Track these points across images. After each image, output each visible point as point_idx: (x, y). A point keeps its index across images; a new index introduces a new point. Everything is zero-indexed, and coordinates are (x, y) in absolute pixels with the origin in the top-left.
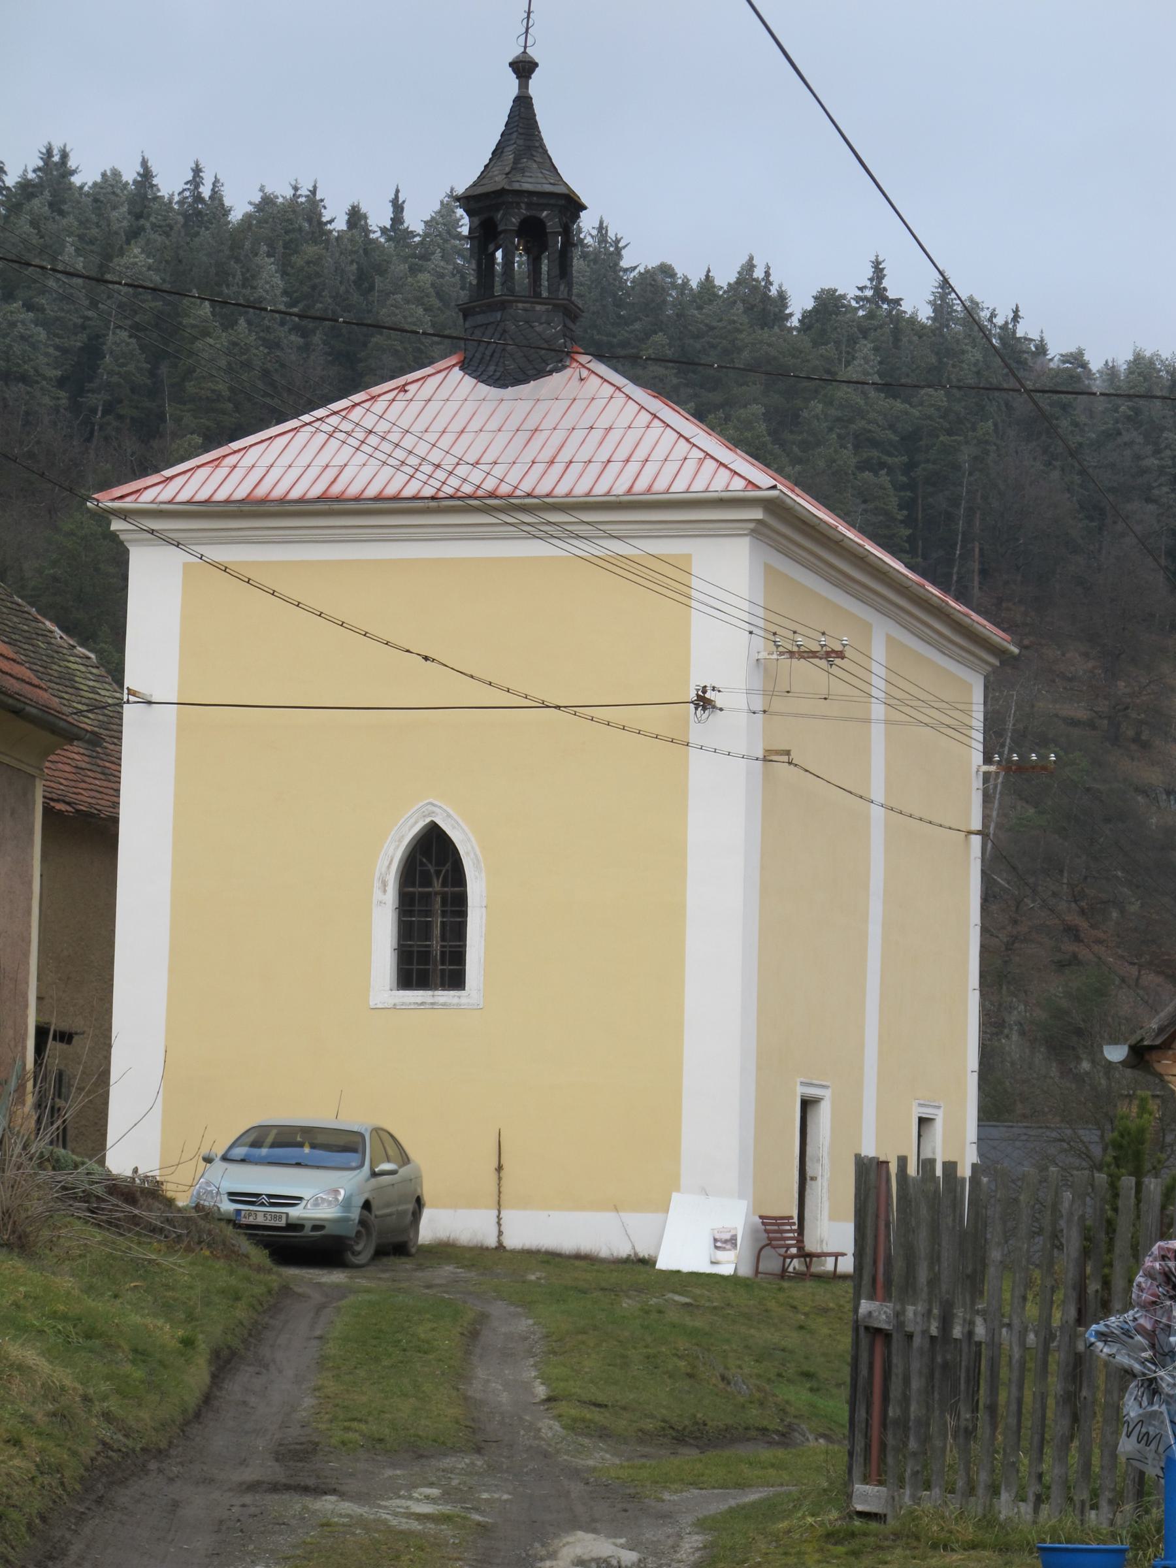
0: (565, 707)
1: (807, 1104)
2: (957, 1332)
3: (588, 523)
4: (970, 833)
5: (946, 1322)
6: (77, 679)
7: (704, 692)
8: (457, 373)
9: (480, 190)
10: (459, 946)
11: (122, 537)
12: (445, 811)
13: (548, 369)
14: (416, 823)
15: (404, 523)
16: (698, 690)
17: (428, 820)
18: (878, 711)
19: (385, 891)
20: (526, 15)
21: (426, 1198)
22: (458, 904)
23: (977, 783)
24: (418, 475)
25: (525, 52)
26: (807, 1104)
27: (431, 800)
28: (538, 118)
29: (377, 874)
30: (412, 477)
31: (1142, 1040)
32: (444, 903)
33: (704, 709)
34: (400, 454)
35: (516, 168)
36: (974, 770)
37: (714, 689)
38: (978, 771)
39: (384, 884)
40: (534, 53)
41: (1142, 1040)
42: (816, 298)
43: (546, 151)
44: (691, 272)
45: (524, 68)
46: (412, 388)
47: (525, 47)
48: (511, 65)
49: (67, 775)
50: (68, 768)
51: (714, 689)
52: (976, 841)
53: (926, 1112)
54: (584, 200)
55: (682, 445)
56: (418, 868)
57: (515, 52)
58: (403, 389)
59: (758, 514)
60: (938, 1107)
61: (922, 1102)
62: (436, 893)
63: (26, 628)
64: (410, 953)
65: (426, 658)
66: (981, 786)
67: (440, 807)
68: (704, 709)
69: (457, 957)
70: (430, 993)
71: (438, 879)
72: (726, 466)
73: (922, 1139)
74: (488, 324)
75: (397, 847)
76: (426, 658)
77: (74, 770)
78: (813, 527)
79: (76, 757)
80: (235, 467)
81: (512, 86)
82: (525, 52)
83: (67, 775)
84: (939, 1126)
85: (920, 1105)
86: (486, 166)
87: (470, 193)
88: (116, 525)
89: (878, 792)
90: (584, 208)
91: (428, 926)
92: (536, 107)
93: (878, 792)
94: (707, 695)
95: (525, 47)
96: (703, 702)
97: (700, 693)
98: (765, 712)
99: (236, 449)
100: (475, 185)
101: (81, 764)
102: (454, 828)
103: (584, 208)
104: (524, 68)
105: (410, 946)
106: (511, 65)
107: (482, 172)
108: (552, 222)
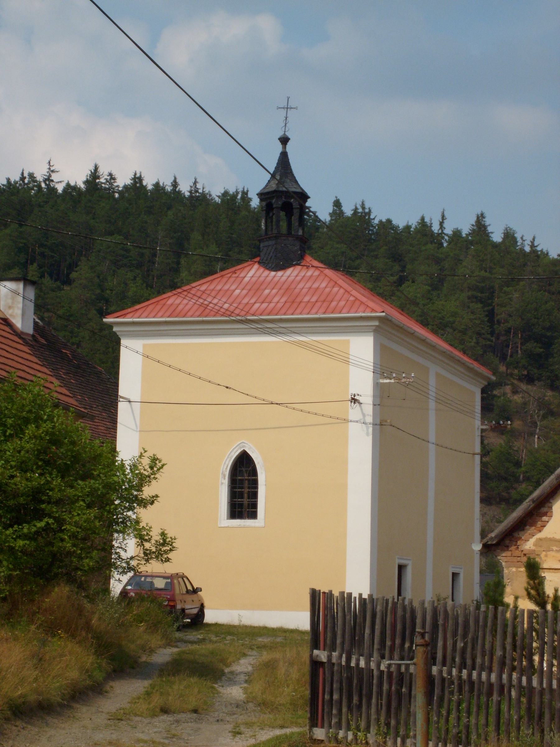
0: (281, 404)
1: (401, 568)
2: (353, 664)
3: (283, 328)
4: (474, 454)
5: (349, 660)
6: (110, 391)
7: (355, 396)
8: (256, 266)
9: (266, 191)
10: (255, 501)
11: (118, 334)
12: (249, 446)
13: (294, 263)
14: (237, 451)
15: (324, 325)
16: (351, 395)
17: (242, 449)
18: (432, 405)
19: (225, 479)
20: (285, 118)
21: (206, 604)
22: (254, 483)
23: (478, 433)
24: (208, 307)
25: (285, 134)
26: (401, 568)
27: (244, 441)
28: (290, 161)
29: (221, 472)
30: (206, 308)
31: (488, 542)
32: (249, 484)
33: (355, 403)
34: (201, 301)
35: (280, 182)
36: (477, 427)
37: (358, 395)
38: (478, 428)
39: (224, 476)
40: (288, 134)
41: (488, 542)
42: (453, 231)
43: (293, 175)
44: (400, 222)
45: (284, 140)
46: (238, 272)
47: (285, 132)
48: (279, 139)
49: (102, 431)
50: (103, 428)
51: (358, 395)
52: (478, 458)
53: (456, 570)
54: (309, 194)
55: (346, 295)
56: (238, 469)
57: (280, 134)
58: (234, 272)
59: (377, 323)
60: (461, 568)
61: (453, 566)
62: (246, 479)
63: (89, 371)
64: (235, 504)
65: (227, 387)
66: (480, 434)
67: (247, 444)
68: (355, 403)
69: (254, 506)
70: (243, 521)
71: (246, 474)
72: (364, 303)
73: (454, 581)
74: (269, 246)
75: (230, 460)
76: (227, 387)
77: (106, 429)
78: (401, 328)
79: (107, 423)
80: (164, 304)
81: (279, 148)
82: (285, 134)
83: (102, 431)
84: (461, 576)
85: (453, 567)
86: (269, 181)
87: (262, 192)
88: (115, 329)
89: (432, 438)
90: (309, 198)
91: (252, 479)
92: (289, 156)
93: (432, 438)
94: (356, 398)
95: (285, 132)
96: (354, 400)
97: (353, 397)
98: (379, 405)
99: (165, 297)
100: (264, 188)
101: (108, 427)
102: (253, 452)
103: (309, 198)
104: (284, 140)
105: (235, 501)
106: (279, 139)
107: (267, 183)
108: (295, 205)
